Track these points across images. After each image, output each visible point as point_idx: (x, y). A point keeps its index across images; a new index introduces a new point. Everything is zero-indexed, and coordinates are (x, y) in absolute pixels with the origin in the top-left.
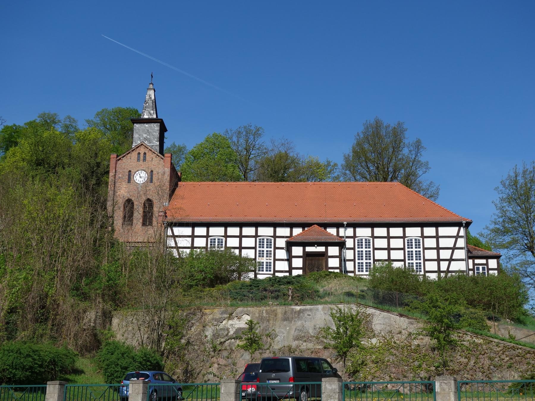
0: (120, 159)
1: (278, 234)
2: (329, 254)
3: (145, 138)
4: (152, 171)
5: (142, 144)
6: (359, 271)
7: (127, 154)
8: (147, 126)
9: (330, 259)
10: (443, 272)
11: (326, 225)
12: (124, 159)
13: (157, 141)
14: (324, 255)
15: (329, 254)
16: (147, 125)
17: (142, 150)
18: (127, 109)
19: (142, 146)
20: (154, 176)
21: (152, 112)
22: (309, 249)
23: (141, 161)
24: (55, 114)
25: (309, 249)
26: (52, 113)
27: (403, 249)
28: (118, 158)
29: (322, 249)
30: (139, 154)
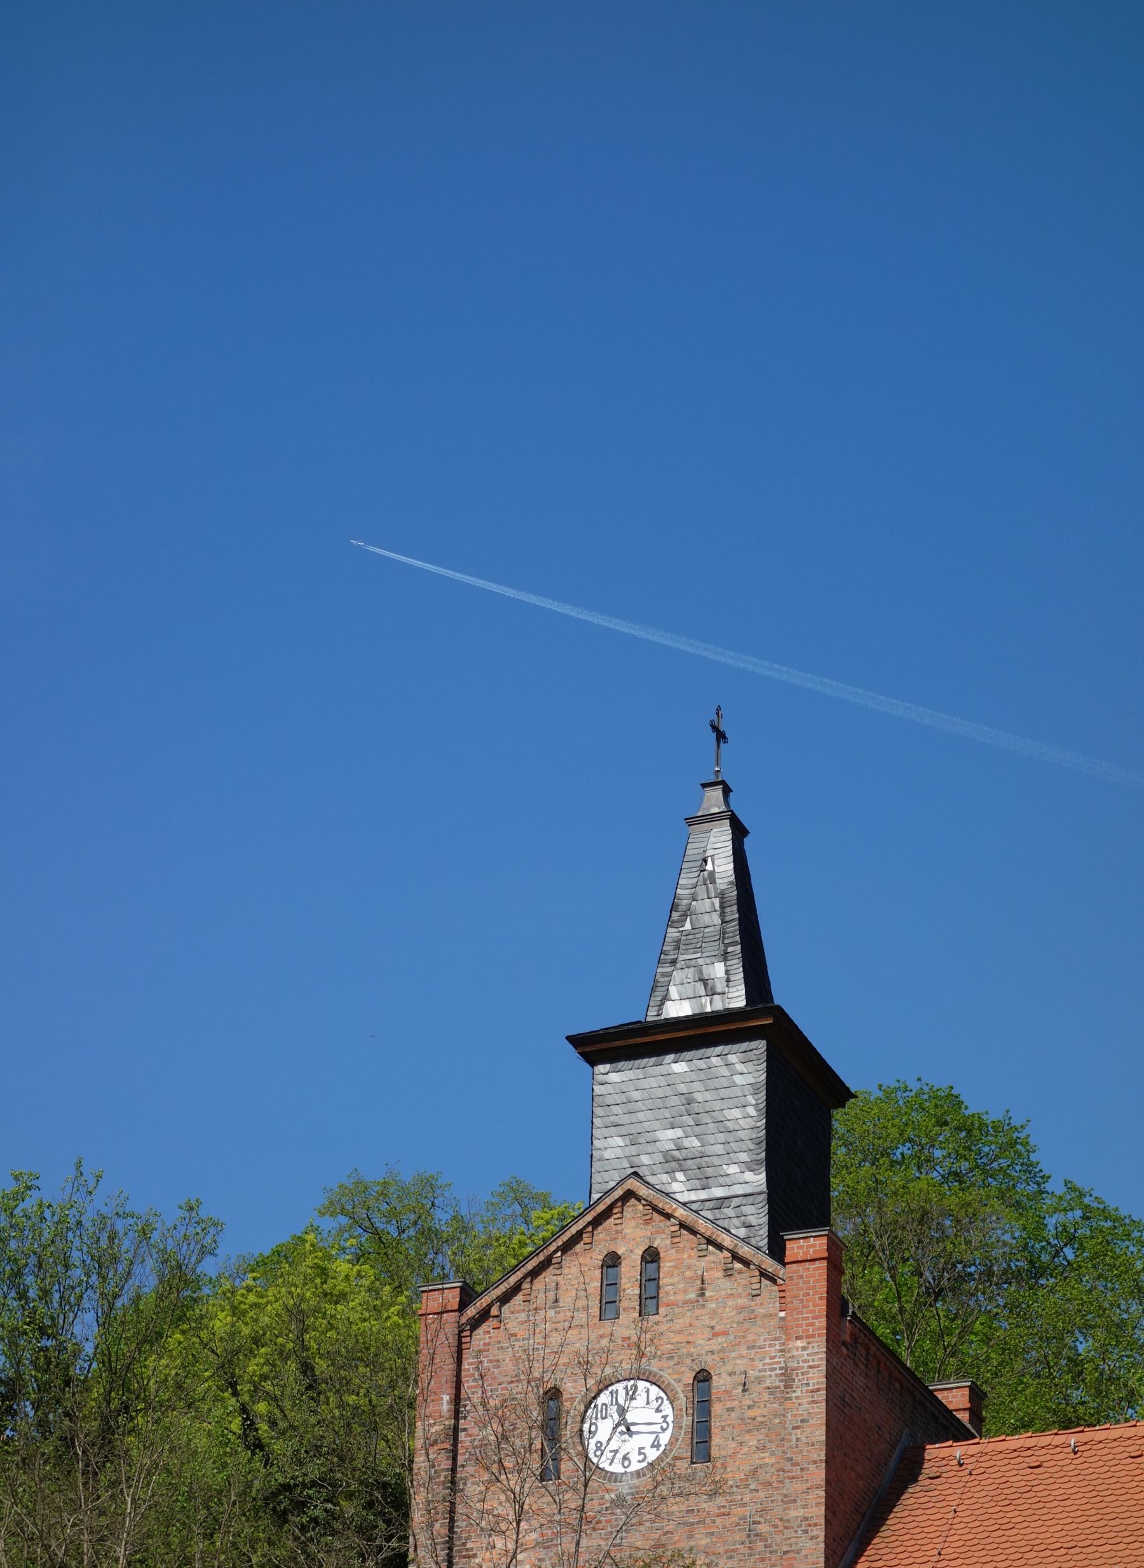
0: (484, 1315)
3: (668, 1158)
4: (703, 1377)
5: (629, 1195)
7: (534, 1274)
8: (680, 1067)
12: (515, 1314)
13: (750, 1167)
16: (678, 1066)
17: (630, 1235)
18: (889, 1095)
19: (634, 1209)
20: (717, 1408)
21: (719, 969)
23: (628, 1316)
24: (429, 1183)
26: (407, 1176)
28: (471, 1312)
30: (612, 1261)
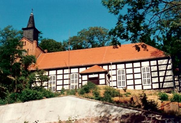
1: (127, 67)
2: (100, 78)
6: (150, 83)
9: (100, 80)
10: (161, 82)
11: (102, 65)
14: (97, 79)
15: (100, 78)
22: (90, 76)
25: (90, 76)
27: (141, 73)
29: (96, 76)
